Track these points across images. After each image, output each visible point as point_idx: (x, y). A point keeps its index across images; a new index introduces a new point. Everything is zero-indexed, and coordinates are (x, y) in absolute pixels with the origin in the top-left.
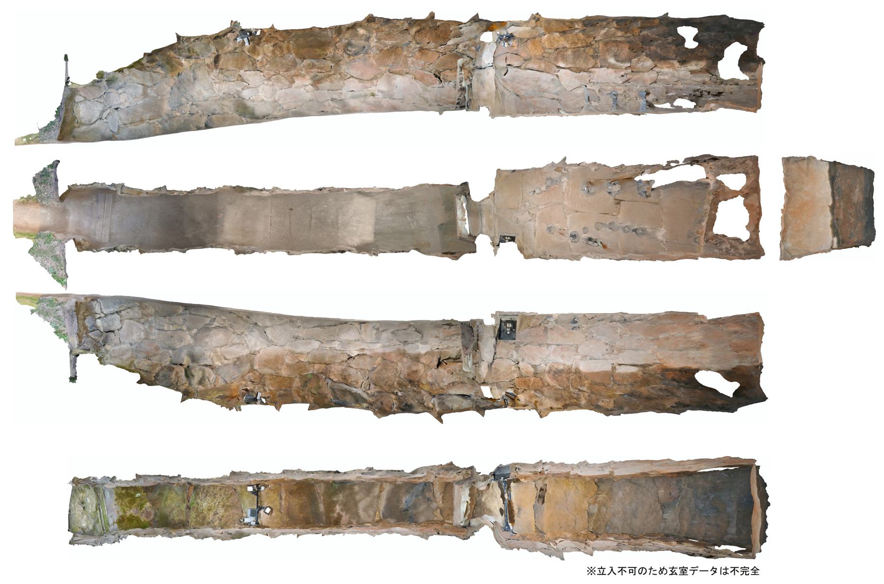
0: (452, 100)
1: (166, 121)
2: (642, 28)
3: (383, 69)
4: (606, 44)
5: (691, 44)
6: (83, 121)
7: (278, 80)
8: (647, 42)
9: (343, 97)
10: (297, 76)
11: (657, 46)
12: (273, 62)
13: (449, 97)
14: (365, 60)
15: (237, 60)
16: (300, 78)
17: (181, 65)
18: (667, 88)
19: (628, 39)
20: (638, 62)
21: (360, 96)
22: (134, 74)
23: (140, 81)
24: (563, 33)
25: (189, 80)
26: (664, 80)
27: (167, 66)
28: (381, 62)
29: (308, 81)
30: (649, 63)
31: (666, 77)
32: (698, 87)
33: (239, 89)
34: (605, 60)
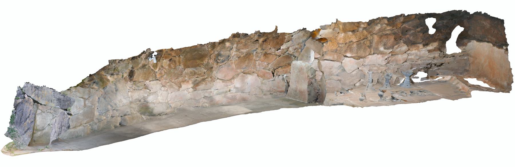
0: (280, 90)
1: (96, 124)
2: (403, 22)
3: (239, 71)
4: (381, 37)
5: (432, 31)
6: (38, 128)
7: (171, 86)
8: (405, 31)
9: (211, 95)
10: (183, 82)
11: (410, 35)
12: (168, 73)
13: (278, 87)
14: (229, 65)
15: (145, 74)
16: (185, 83)
17: (108, 80)
18: (411, 64)
19: (393, 32)
20: (397, 48)
21: (223, 93)
22: (79, 91)
23: (81, 96)
24: (353, 31)
25: (112, 92)
26: (411, 59)
27: (101, 83)
28: (238, 66)
29: (190, 85)
30: (405, 48)
31: (413, 57)
32: (430, 62)
33: (146, 95)
34: (377, 49)
